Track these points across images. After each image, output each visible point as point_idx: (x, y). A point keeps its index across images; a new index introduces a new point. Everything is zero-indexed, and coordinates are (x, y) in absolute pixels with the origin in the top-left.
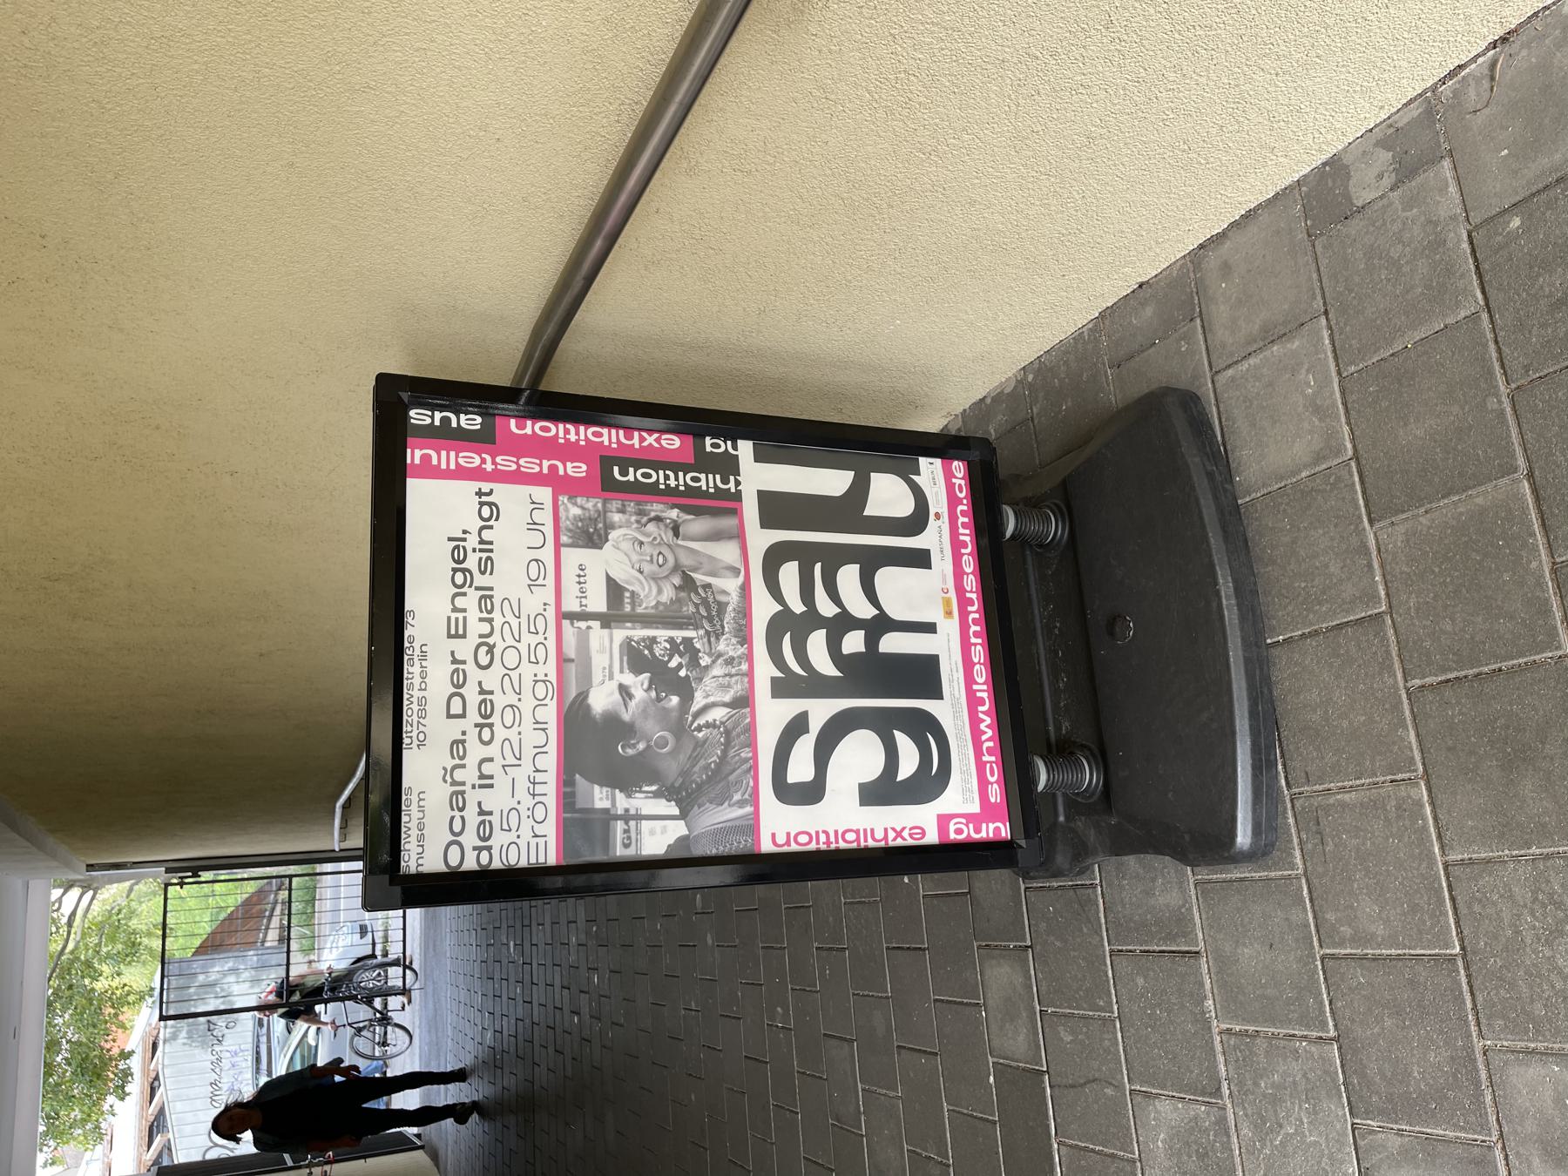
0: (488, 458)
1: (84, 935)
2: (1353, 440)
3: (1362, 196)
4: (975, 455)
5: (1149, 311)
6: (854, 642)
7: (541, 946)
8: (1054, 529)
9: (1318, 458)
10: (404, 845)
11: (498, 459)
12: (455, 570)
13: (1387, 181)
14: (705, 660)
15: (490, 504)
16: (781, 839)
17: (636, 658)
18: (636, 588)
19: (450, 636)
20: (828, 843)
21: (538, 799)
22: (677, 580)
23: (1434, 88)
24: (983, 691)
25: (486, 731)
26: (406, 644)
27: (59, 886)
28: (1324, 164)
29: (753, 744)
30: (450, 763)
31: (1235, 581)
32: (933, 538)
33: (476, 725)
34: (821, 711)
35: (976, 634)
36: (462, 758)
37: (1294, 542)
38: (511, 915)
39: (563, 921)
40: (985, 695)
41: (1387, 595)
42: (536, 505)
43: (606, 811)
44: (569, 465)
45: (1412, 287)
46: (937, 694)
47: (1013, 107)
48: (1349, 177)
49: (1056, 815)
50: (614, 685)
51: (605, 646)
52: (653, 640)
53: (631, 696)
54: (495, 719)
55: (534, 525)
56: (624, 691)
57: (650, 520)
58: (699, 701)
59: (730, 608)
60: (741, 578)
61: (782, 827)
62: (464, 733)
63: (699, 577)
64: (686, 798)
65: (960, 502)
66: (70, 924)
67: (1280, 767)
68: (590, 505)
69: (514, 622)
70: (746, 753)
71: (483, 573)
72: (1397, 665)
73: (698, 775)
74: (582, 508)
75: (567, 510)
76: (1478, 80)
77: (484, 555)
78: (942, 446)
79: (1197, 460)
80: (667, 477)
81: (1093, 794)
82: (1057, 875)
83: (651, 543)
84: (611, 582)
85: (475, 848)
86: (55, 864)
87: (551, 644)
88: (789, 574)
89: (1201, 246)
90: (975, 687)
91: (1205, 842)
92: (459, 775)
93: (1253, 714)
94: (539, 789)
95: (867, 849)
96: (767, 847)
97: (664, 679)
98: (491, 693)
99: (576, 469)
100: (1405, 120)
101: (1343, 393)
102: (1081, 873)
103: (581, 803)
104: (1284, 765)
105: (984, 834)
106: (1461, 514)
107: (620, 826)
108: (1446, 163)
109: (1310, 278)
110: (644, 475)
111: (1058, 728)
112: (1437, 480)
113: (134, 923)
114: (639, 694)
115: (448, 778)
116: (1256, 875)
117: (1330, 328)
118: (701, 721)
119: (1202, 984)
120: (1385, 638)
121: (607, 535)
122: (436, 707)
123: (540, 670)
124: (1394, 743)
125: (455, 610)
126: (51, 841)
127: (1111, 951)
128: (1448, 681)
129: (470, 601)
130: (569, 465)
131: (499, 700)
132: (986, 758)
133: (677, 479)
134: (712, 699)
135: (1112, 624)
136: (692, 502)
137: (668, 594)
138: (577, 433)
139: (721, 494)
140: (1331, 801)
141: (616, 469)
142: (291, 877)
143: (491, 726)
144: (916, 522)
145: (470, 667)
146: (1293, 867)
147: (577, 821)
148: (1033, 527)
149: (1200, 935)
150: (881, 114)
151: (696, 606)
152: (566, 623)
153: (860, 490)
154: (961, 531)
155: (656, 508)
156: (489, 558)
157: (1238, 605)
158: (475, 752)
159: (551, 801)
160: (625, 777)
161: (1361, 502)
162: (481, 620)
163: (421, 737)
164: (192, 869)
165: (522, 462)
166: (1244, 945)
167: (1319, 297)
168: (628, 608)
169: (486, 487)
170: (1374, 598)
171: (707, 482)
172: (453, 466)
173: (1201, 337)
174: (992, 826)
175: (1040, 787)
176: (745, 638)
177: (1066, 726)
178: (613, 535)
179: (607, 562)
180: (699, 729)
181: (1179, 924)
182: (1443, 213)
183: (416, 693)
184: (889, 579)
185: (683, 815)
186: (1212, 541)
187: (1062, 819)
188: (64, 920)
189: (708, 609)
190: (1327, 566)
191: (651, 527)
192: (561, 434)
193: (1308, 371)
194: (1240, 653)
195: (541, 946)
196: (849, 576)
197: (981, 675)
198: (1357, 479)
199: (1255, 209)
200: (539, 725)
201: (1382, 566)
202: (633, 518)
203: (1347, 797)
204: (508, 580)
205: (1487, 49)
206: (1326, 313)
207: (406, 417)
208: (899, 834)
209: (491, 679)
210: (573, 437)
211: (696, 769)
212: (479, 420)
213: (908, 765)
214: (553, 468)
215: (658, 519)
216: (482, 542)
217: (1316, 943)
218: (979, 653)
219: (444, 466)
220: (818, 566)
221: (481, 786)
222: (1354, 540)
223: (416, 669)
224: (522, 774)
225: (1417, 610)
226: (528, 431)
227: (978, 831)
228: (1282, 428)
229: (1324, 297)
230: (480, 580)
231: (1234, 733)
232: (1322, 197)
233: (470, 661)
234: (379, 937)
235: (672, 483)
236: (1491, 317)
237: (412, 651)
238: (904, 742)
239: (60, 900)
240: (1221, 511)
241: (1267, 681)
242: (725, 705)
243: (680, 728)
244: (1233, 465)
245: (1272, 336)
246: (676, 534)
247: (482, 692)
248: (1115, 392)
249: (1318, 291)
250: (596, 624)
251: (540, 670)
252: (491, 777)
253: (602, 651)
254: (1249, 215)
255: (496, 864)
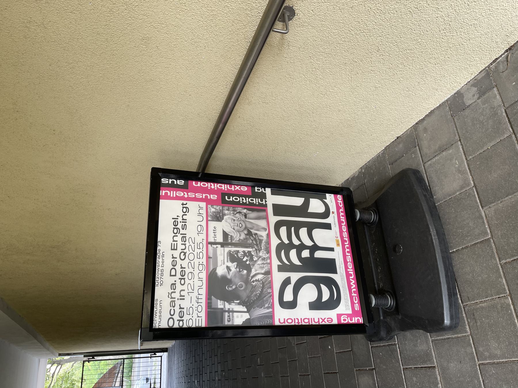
0: (186, 193)
1: (57, 380)
2: (473, 181)
3: (468, 102)
4: (345, 193)
5: (401, 146)
6: (306, 254)
7: (206, 381)
8: (373, 217)
9: (462, 188)
10: (155, 319)
11: (189, 194)
12: (174, 228)
13: (476, 97)
14: (255, 259)
15: (186, 208)
16: (282, 321)
17: (233, 257)
18: (233, 234)
19: (172, 249)
20: (298, 322)
21: (199, 304)
22: (246, 232)
23: (489, 66)
24: (351, 271)
25: (183, 281)
26: (158, 252)
27: (50, 364)
28: (455, 94)
29: (271, 287)
30: (170, 291)
31: (436, 230)
32: (332, 219)
33: (179, 279)
34: (295, 277)
35: (348, 252)
36: (174, 289)
37: (456, 216)
38: (196, 370)
39: (213, 372)
40: (352, 273)
41: (491, 232)
42: (201, 208)
43: (222, 309)
44: (211, 195)
45: (488, 129)
46: (335, 272)
47: (350, 78)
48: (463, 97)
49: (380, 317)
50: (225, 266)
51: (222, 253)
52: (238, 251)
53: (230, 270)
54: (186, 277)
55: (200, 214)
56: (228, 268)
57: (237, 213)
58: (253, 272)
59: (263, 241)
60: (267, 232)
61: (282, 317)
62: (175, 281)
63: (253, 231)
64: (249, 306)
65: (341, 208)
66: (53, 377)
67: (459, 296)
68: (218, 208)
69: (193, 245)
70: (269, 291)
71: (183, 229)
72: (496, 256)
73: (253, 298)
74: (215, 209)
75: (210, 209)
76: (503, 62)
77: (184, 224)
78: (334, 190)
79: (420, 191)
80: (243, 200)
81: (392, 308)
82: (381, 339)
83: (237, 220)
84: (224, 232)
85: (178, 320)
86: (48, 352)
87: (205, 252)
88: (283, 230)
89: (417, 124)
90: (348, 270)
91: (433, 324)
92: (173, 295)
93: (447, 276)
94: (200, 301)
95: (312, 325)
96: (277, 323)
97: (241, 265)
98: (185, 268)
99: (214, 197)
100: (480, 78)
101: (468, 166)
102: (390, 339)
103: (213, 306)
104: (460, 295)
105: (353, 321)
106: (513, 202)
107: (227, 314)
108: (495, 89)
109: (454, 130)
110: (235, 199)
111: (379, 286)
112: (503, 191)
113: (73, 377)
114: (233, 269)
115: (170, 296)
116: (454, 336)
117: (462, 145)
118: (254, 279)
119: (437, 379)
120: (491, 247)
121: (223, 217)
122: (166, 273)
123: (201, 261)
124: (498, 284)
125: (174, 241)
126: (47, 344)
127: (403, 368)
128: (515, 260)
129: (179, 238)
130: (211, 195)
131: (187, 271)
132: (353, 294)
133: (246, 200)
134: (257, 272)
135: (395, 248)
136: (251, 207)
137: (243, 236)
138: (214, 186)
139: (260, 205)
140: (478, 306)
141: (226, 197)
142: (124, 359)
143: (184, 279)
144: (326, 214)
145: (178, 260)
146: (466, 332)
147: (212, 313)
148: (366, 216)
149: (435, 360)
150: (308, 82)
151: (252, 240)
152: (209, 245)
153: (306, 204)
154: (341, 217)
155: (239, 209)
156: (185, 225)
157: (438, 238)
158: (179, 287)
159: (204, 305)
160: (229, 297)
161: (478, 201)
162: (182, 244)
163: (162, 282)
164: (92, 356)
165: (196, 195)
166: (451, 362)
167: (457, 135)
168: (230, 241)
169: (185, 202)
170: (486, 233)
171: (256, 201)
172: (175, 196)
173: (419, 152)
174: (356, 319)
175: (373, 305)
176: (268, 251)
177: (381, 285)
178: (225, 217)
179: (223, 226)
180: (253, 282)
181: (427, 357)
182: (496, 104)
183: (160, 268)
184: (316, 232)
185: (248, 311)
186: (427, 217)
187: (382, 318)
188: (51, 375)
189: (256, 242)
190: (468, 224)
191: (238, 215)
192: (209, 186)
193: (456, 160)
194: (440, 255)
195: (206, 381)
196: (303, 232)
197: (350, 266)
198: (476, 193)
199: (433, 110)
200: (200, 279)
201: (488, 222)
202: (232, 212)
203: (483, 305)
204: (191, 231)
205: (505, 52)
206: (460, 140)
207: (160, 181)
208: (323, 320)
209: (185, 264)
210: (213, 187)
211: (253, 295)
212: (183, 182)
213: (326, 296)
214: (206, 197)
215: (240, 213)
216: (183, 219)
217: (476, 360)
218: (349, 258)
219: (172, 196)
220: (293, 228)
221: (180, 299)
222: (477, 214)
223: (161, 260)
224: (194, 295)
225: (501, 236)
226: (199, 185)
227: (351, 320)
228: (449, 178)
229: (459, 135)
230: (182, 231)
231: (440, 283)
232: (455, 104)
233: (178, 258)
234: (152, 381)
235: (245, 201)
236: (515, 136)
237: (159, 254)
238: (324, 288)
239: (50, 368)
240: (430, 208)
241: (451, 264)
242: (262, 274)
243: (247, 281)
244: (433, 193)
245: (442, 149)
246: (246, 217)
247: (182, 268)
248: (391, 171)
249: (457, 134)
250: (219, 246)
251: (201, 261)
252: (184, 296)
253: (221, 255)
254: (432, 112)
255: (185, 326)
